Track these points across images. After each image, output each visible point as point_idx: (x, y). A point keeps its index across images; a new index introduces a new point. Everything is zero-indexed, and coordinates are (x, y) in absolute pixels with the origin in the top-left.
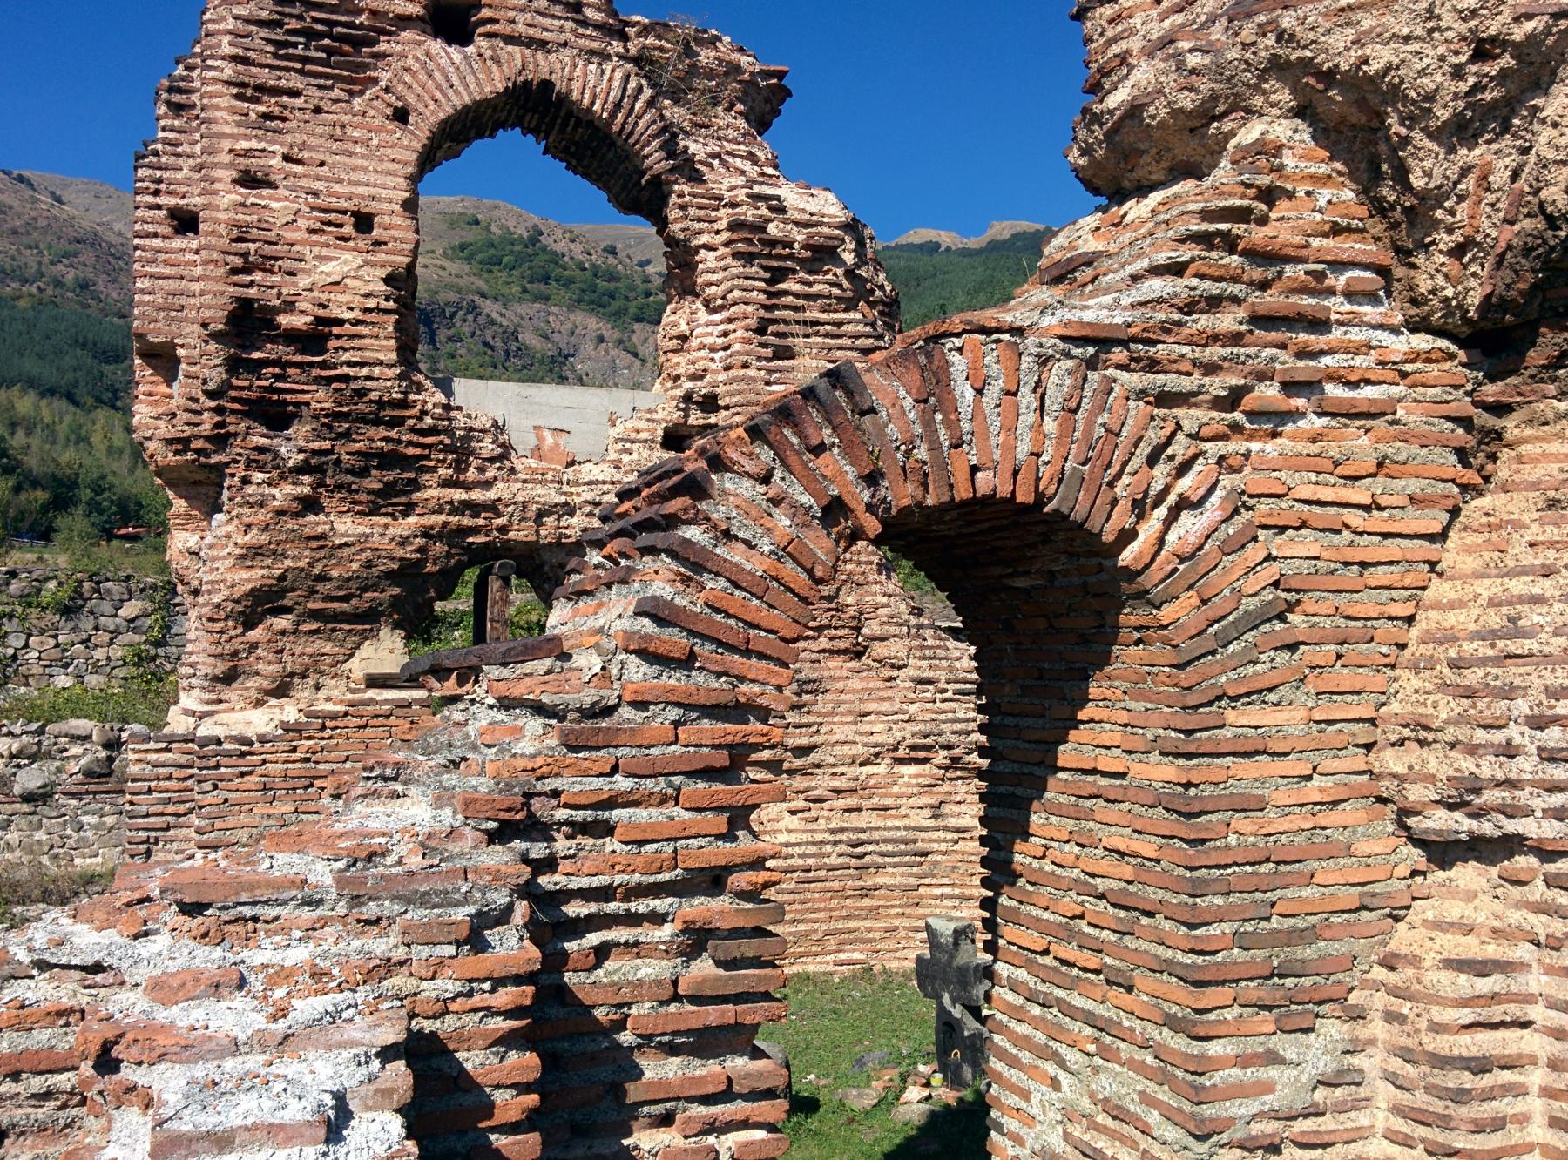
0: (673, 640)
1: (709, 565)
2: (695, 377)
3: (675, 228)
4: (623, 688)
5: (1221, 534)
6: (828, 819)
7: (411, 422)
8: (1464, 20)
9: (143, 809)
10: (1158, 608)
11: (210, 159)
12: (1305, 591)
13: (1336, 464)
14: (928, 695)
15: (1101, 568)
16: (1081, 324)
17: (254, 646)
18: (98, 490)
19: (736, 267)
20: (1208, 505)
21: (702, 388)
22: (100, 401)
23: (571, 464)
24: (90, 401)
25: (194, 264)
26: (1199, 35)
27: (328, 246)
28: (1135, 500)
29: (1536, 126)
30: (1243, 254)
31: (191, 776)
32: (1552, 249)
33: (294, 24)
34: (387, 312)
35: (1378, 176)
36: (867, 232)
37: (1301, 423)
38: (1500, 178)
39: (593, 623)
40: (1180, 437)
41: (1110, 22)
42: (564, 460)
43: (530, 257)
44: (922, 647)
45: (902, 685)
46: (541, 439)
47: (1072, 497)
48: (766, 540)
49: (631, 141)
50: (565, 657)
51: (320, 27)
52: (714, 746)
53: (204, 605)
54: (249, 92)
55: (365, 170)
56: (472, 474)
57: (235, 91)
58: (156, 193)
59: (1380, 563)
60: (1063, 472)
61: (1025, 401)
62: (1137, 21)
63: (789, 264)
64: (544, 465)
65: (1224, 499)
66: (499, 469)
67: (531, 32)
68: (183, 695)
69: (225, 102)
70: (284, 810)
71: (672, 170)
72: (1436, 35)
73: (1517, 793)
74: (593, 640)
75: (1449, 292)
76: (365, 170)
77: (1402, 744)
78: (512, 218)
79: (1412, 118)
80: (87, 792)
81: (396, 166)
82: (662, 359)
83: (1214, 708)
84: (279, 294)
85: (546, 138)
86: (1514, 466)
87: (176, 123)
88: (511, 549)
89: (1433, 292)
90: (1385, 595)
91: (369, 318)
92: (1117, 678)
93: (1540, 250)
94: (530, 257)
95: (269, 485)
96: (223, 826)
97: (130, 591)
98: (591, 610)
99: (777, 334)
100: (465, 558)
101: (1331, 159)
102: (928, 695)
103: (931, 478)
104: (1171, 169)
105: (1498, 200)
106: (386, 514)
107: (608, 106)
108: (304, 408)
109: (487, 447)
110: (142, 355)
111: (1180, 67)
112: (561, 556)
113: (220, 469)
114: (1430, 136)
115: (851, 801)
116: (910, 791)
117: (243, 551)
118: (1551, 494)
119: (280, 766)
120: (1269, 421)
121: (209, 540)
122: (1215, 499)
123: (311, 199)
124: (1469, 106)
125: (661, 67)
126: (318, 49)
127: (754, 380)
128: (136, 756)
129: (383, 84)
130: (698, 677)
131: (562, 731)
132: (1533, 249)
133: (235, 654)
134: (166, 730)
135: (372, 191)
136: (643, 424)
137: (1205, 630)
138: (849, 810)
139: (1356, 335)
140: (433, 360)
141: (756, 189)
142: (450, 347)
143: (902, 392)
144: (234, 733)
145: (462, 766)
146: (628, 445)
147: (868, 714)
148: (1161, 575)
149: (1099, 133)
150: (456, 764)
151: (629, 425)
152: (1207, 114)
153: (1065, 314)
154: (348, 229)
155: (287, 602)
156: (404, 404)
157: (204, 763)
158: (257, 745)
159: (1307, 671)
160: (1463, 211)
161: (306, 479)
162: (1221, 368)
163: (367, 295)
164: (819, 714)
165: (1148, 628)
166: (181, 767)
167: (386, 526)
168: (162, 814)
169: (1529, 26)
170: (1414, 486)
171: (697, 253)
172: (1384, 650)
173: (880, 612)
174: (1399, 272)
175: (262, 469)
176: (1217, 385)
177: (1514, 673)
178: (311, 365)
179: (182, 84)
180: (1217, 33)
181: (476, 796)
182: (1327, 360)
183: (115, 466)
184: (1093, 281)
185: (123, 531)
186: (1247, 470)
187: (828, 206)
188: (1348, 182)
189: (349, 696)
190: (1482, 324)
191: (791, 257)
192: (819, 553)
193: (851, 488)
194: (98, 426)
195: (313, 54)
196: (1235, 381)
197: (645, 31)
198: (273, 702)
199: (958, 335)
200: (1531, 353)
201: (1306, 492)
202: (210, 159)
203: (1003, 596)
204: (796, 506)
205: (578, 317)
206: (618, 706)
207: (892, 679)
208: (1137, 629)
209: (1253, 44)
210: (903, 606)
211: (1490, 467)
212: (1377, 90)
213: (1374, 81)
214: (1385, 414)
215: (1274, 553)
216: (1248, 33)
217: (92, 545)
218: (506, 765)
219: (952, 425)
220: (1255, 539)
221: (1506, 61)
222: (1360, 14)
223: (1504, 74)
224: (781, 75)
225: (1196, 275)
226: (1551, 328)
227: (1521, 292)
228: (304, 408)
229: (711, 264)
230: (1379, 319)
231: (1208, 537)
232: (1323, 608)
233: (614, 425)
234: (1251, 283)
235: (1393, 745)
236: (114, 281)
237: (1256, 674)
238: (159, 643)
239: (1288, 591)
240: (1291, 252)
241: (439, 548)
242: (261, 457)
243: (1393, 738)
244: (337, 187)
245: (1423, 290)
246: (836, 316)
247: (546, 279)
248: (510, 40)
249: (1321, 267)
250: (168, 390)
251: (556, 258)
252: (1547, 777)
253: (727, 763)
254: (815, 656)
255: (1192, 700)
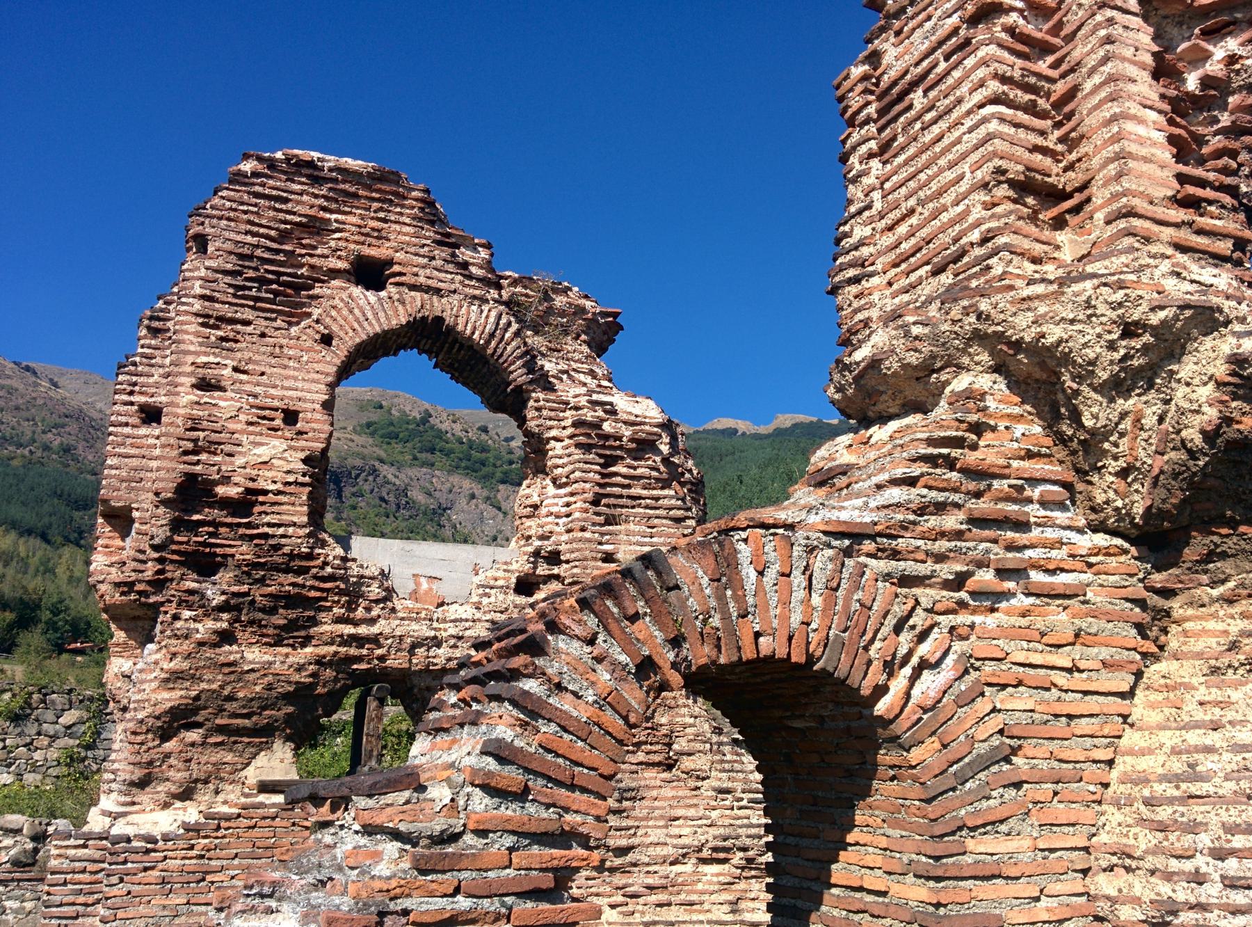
0: (512, 776)
1: (543, 713)
2: (543, 537)
3: (532, 425)
4: (468, 817)
5: (955, 690)
6: (643, 913)
7: (314, 571)
8: (1114, 309)
9: (57, 899)
10: (908, 751)
11: (176, 369)
12: (1025, 738)
13: (1043, 635)
14: (727, 803)
15: (861, 716)
16: (839, 522)
17: (168, 756)
18: (56, 611)
19: (578, 454)
20: (943, 666)
21: (548, 546)
22: (67, 540)
23: (441, 604)
24: (59, 540)
25: (155, 446)
26: (919, 311)
27: (261, 434)
28: (885, 661)
29: (1174, 385)
30: (960, 471)
31: (103, 870)
32: (1195, 474)
33: (251, 274)
34: (303, 485)
35: (1058, 417)
36: (679, 430)
37: (1013, 601)
38: (1150, 421)
39: (447, 758)
40: (919, 611)
41: (856, 297)
42: (436, 601)
43: (421, 434)
44: (722, 761)
45: (706, 794)
46: (418, 584)
47: (835, 659)
48: (591, 692)
49: (501, 361)
50: (421, 788)
51: (270, 276)
52: (541, 870)
53: (130, 720)
54: (212, 321)
55: (296, 379)
56: (360, 613)
57: (201, 320)
58: (131, 393)
59: (1082, 716)
60: (827, 638)
61: (796, 582)
62: (875, 297)
63: (619, 453)
64: (418, 605)
65: (957, 661)
66: (383, 609)
67: (430, 282)
68: (103, 797)
69: (192, 328)
70: (178, 901)
71: (531, 382)
72: (1094, 319)
73: (1207, 915)
74: (446, 774)
75: (1119, 503)
76: (296, 379)
77: (1112, 870)
78: (408, 404)
79: (1080, 377)
80: (13, 880)
81: (319, 376)
82: (518, 522)
83: (956, 838)
84: (219, 471)
85: (436, 357)
86: (1182, 639)
87: (153, 342)
88: (387, 675)
89: (1107, 502)
90: (1089, 742)
91: (292, 489)
92: (877, 808)
93: (1186, 475)
94: (421, 434)
95: (195, 621)
96: (125, 916)
97: (71, 702)
98: (446, 745)
99: (608, 506)
100: (349, 682)
101: (1022, 403)
102: (727, 803)
103: (723, 641)
104: (903, 405)
105: (1150, 437)
106: (288, 645)
107: (485, 336)
108: (230, 559)
109: (375, 591)
110: (104, 516)
111: (907, 334)
112: (429, 681)
113: (156, 607)
114: (1095, 390)
115: (662, 897)
116: (712, 888)
117: (167, 676)
118: (1213, 662)
119: (178, 862)
120: (988, 599)
121: (139, 666)
122: (950, 660)
123: (251, 400)
124: (1122, 369)
125: (526, 309)
126: (267, 291)
127: (589, 541)
128: (57, 852)
129: (315, 317)
130: (531, 809)
131: (414, 856)
132: (1180, 473)
133: (150, 763)
134: (86, 829)
135: (299, 394)
136: (500, 574)
137: (945, 771)
138: (660, 905)
139: (1051, 534)
140: (339, 511)
141: (595, 397)
142: (353, 500)
143: (700, 573)
144: (142, 832)
145: (329, 885)
146: (487, 590)
147: (677, 819)
148: (909, 724)
149: (849, 377)
150: (323, 883)
151: (489, 574)
152: (927, 369)
153: (825, 514)
154: (278, 422)
155: (199, 718)
156: (310, 557)
157: (115, 859)
158: (161, 843)
159: (1030, 806)
160: (1124, 443)
161: (225, 616)
162: (948, 557)
163: (288, 472)
164: (636, 819)
165: (900, 767)
166: (95, 861)
167: (287, 655)
168: (73, 904)
169: (1162, 315)
170: (1105, 653)
171: (548, 443)
172: (1092, 788)
173: (688, 730)
174: (1080, 487)
175: (190, 608)
176: (946, 571)
177: (1196, 811)
178: (239, 525)
179: (161, 314)
180: (933, 311)
181: (338, 915)
182: (1029, 553)
183: (72, 592)
184: (848, 486)
185: (73, 646)
186: (973, 638)
187: (649, 411)
188: (1036, 420)
189: (243, 800)
190: (1146, 528)
191: (620, 448)
192: (633, 703)
193: (659, 649)
194: (63, 560)
195: (264, 295)
196: (959, 568)
197: (515, 283)
198: (178, 804)
199: (744, 529)
200: (1186, 550)
201: (1020, 657)
202: (176, 369)
203: (784, 734)
204: (615, 665)
205: (455, 479)
206: (463, 833)
207: (697, 788)
208: (892, 767)
209: (960, 320)
210: (706, 726)
211: (1163, 638)
212: (1053, 356)
213: (1050, 349)
214: (1077, 595)
215: (999, 706)
216: (956, 313)
217: (45, 658)
218: (365, 886)
219: (740, 599)
220: (982, 694)
221: (1147, 338)
222: (1036, 303)
223: (1146, 348)
224: (616, 315)
225: (925, 487)
226: (1200, 532)
227: (1174, 505)
228: (230, 559)
229: (559, 451)
230: (1067, 522)
231: (945, 692)
232: (1039, 753)
233: (477, 574)
234: (968, 493)
235: (1105, 870)
236: (91, 447)
237: (989, 808)
238: (89, 747)
239: (1012, 737)
240: (997, 471)
241: (329, 673)
242: (191, 598)
243: (1104, 864)
244: (272, 391)
245: (1099, 501)
246: (655, 492)
247: (432, 450)
248: (413, 287)
249: (1020, 482)
250: (121, 544)
251: (440, 434)
252: (1231, 902)
253: (552, 885)
254: (634, 767)
255: (938, 830)
